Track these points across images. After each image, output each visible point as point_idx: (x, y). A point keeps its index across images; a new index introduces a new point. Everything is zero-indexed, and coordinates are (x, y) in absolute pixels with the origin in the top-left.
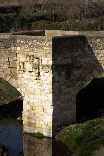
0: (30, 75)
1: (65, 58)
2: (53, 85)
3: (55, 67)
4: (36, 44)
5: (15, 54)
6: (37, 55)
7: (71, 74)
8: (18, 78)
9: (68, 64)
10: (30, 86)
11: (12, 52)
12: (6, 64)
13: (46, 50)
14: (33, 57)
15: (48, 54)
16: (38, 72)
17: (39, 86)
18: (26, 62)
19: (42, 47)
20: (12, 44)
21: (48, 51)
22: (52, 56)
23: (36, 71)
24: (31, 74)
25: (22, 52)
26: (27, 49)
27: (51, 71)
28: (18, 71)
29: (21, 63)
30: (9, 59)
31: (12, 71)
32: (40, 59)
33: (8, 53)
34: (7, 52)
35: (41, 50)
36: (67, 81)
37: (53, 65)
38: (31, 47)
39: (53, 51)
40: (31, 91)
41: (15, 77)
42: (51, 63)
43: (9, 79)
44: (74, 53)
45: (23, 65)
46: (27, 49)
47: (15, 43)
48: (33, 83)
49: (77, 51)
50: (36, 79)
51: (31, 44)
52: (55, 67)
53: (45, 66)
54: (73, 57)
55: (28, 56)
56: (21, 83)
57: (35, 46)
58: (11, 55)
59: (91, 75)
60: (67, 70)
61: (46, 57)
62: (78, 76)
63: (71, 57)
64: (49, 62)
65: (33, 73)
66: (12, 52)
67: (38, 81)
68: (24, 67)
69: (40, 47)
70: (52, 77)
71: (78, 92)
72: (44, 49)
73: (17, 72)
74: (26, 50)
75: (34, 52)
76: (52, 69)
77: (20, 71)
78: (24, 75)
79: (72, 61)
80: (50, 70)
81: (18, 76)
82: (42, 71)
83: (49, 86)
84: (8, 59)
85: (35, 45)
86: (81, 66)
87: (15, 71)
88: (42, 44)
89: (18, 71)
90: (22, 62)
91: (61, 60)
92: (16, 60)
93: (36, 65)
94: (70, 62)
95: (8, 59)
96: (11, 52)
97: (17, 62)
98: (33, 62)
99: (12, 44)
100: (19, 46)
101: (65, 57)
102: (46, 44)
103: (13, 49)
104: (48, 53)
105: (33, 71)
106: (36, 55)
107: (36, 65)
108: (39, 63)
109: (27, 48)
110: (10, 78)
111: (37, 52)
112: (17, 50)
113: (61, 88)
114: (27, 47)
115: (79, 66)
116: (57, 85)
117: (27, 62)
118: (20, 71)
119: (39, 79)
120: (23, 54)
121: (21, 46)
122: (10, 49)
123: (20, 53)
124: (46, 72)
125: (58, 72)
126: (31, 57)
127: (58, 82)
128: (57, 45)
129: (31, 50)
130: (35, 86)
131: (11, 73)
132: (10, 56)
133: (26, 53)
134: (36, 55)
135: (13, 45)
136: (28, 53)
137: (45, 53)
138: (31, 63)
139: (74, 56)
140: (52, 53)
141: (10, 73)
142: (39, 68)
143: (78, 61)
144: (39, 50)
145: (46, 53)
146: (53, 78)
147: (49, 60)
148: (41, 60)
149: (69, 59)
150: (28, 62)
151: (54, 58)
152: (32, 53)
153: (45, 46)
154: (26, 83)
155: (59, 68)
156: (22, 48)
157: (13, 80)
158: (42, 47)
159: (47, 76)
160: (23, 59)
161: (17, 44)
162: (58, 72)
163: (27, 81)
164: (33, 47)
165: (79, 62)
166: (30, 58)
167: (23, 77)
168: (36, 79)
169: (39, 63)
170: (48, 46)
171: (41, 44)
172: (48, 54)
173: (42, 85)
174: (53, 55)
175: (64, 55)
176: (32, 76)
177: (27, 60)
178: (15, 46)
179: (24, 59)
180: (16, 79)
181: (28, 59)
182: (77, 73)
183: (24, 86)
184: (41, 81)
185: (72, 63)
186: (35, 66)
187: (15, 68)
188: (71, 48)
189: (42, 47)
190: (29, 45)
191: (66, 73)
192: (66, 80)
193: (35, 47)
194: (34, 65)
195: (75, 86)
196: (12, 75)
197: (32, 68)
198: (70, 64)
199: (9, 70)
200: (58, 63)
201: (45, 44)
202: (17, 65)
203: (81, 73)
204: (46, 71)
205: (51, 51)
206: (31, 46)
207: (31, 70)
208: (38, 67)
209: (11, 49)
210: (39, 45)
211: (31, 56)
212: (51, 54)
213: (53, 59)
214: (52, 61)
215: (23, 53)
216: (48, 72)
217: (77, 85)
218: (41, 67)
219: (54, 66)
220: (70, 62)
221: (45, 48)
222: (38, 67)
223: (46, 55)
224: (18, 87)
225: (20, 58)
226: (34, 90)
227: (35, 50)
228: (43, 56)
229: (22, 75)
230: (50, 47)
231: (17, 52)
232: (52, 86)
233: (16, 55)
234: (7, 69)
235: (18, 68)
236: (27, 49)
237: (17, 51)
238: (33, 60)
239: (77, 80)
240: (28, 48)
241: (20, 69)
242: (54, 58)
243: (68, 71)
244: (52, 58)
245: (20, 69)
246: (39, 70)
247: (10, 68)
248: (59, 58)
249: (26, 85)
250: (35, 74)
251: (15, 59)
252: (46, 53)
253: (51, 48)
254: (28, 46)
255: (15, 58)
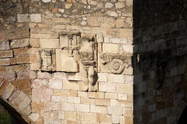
0: (70, 81)
1: (155, 38)
2: (135, 103)
3: (138, 59)
4: (88, 4)
5: (26, 31)
6: (89, 32)
7: (167, 75)
8: (33, 90)
9: (160, 51)
10: (67, 107)
11: (19, 26)
12: (4, 55)
13: (116, 19)
14: (78, 37)
15: (121, 29)
16: (93, 73)
17: (93, 107)
18: (57, 51)
19: (103, 13)
20: (19, 6)
21: (120, 22)
22: (132, 34)
23: (87, 71)
24: (71, 78)
25: (45, 26)
26: (62, 17)
27: (130, 70)
28: (35, 73)
29: (43, 53)
30: (12, 44)
31: (19, 73)
32: (99, 40)
33: (8, 28)
34: (6, 25)
35: (100, 19)
36: (159, 93)
37: (134, 54)
38: (71, 14)
39: (134, 20)
40: (71, 119)
41: (26, 87)
42: (129, 49)
43: (10, 93)
44: (170, 24)
45: (51, 58)
46: (60, 17)
47: (26, 5)
48: (77, 100)
49: (176, 20)
50: (87, 91)
51: (71, 5)
52: (138, 59)
53: (113, 58)
54: (169, 34)
55: (66, 35)
56: (42, 101)
57: (83, 9)
58: (16, 35)
59: (111, 73)
60: (158, 66)
61: (115, 35)
62: (178, 79)
63: (165, 34)
64: (124, 47)
65: (76, 77)
66: (19, 26)
67: (93, 95)
68: (52, 62)
69: (97, 13)
70: (132, 83)
71: (179, 118)
72: (109, 16)
73: (32, 75)
74: (57, 22)
75: (80, 25)
76: (133, 66)
77: (39, 73)
78: (51, 81)
79: (168, 44)
80: (127, 66)
81: (33, 85)
82: (104, 71)
83: (123, 105)
84: (10, 44)
85: (85, 7)
86: (183, 56)
87: (27, 73)
88: (104, 6)
89: (32, 72)
90: (49, 50)
91: (148, 43)
92: (29, 47)
93: (87, 56)
94: (164, 47)
95: (10, 44)
96: (16, 26)
97: (32, 51)
98: (77, 49)
99: (19, 6)
100: (38, 12)
101: (154, 34)
102: (116, 4)
103: (21, 18)
104: (121, 26)
105: (78, 72)
106: (86, 32)
107: (89, 56)
108: (95, 51)
109: (59, 15)
110: (14, 91)
111: (90, 24)
112: (33, 21)
113: (149, 111)
114: (60, 13)
115: (180, 55)
116: (141, 102)
117: (63, 49)
118: (39, 73)
119: (95, 90)
120: (49, 32)
121: (41, 10)
122: (13, 19)
123: (41, 29)
124: (115, 72)
125: (143, 72)
126: (74, 37)
127: (143, 94)
128: (140, 7)
129: (72, 20)
130: (85, 108)
131: (16, 77)
132: (14, 37)
133: (59, 28)
134: (86, 32)
135: (21, 9)
136: (63, 27)
137: (113, 25)
138: (72, 52)
139: (171, 32)
140: (131, 26)
141: (14, 79)
142: (95, 63)
143: (178, 43)
144: (93, 20)
145: (115, 27)
146: (135, 87)
147: (125, 42)
148: (99, 45)
149: (161, 38)
150: (64, 51)
151: (137, 37)
152: (75, 28)
153: (114, 9)
154: (58, 101)
155: (145, 61)
156: (47, 17)
157: (22, 94)
158: (103, 13)
159: (117, 81)
160: (48, 43)
161: (30, 7)
162: (144, 70)
163: (58, 97)
164: (80, 12)
165: (180, 46)
166: (71, 39)
167: (47, 87)
168: (87, 91)
169: (95, 51)
170: (122, 9)
171: (100, 6)
172: (122, 28)
173: (105, 104)
174: (134, 32)
175: (154, 29)
176: (74, 84)
177: (63, 45)
178: (26, 11)
179: (84, 43)
180: (28, 92)
181: (65, 42)
182: (176, 74)
183: (50, 109)
184: (101, 95)
185: (166, 48)
186: (85, 58)
187: (25, 65)
188: (166, 12)
189: (103, 12)
190: (65, 9)
191: (158, 73)
192: (158, 91)
193: (85, 12)
194: (84, 56)
195: (171, 105)
196: (20, 83)
197: (75, 65)
198: (165, 50)
199: (10, 71)
200: (143, 49)
201: (113, 5)
202: (31, 58)
203: (182, 72)
204: (117, 70)
205: (130, 21)
206: (71, 9)
207: (74, 69)
208: (93, 60)
209: (17, 20)
210: (95, 6)
211: (73, 35)
212: (129, 28)
213: (134, 40)
214: (133, 44)
215: (48, 28)
216: (122, 71)
217: (176, 103)
218: (100, 62)
219: (136, 57)
220: (164, 47)
221: (113, 14)
222: (93, 62)
223: (116, 32)
224: (33, 111)
225: (41, 40)
226: (80, 116)
227: (85, 19)
228: (108, 33)
229: (44, 82)
230: (126, 12)
231: (31, 26)
232: (131, 105)
233: (28, 34)
234: (7, 68)
235: (34, 66)
236: (60, 17)
237: (30, 24)
238: (78, 45)
239: (176, 89)
240: (65, 16)
241: (41, 66)
242: (137, 37)
243: (161, 68)
244: (132, 39)
245: (41, 66)
246: (95, 67)
247: (13, 65)
248: (144, 39)
249: (56, 107)
250: (84, 79)
251: (26, 44)
252: (115, 27)
253: (131, 15)
254: (62, 11)
255: (27, 40)
